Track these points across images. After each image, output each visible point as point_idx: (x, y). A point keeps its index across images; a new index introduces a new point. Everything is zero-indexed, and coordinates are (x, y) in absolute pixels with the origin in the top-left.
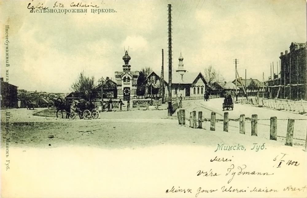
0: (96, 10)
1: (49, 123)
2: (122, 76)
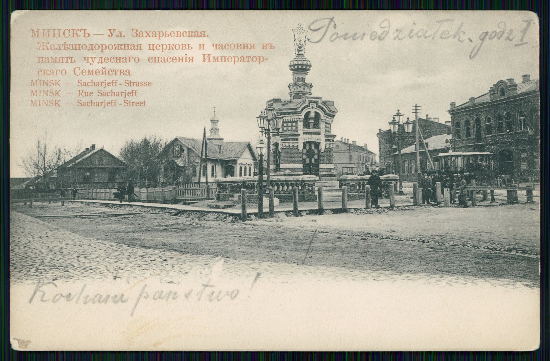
0: (158, 46)
1: (401, 253)
2: (302, 110)
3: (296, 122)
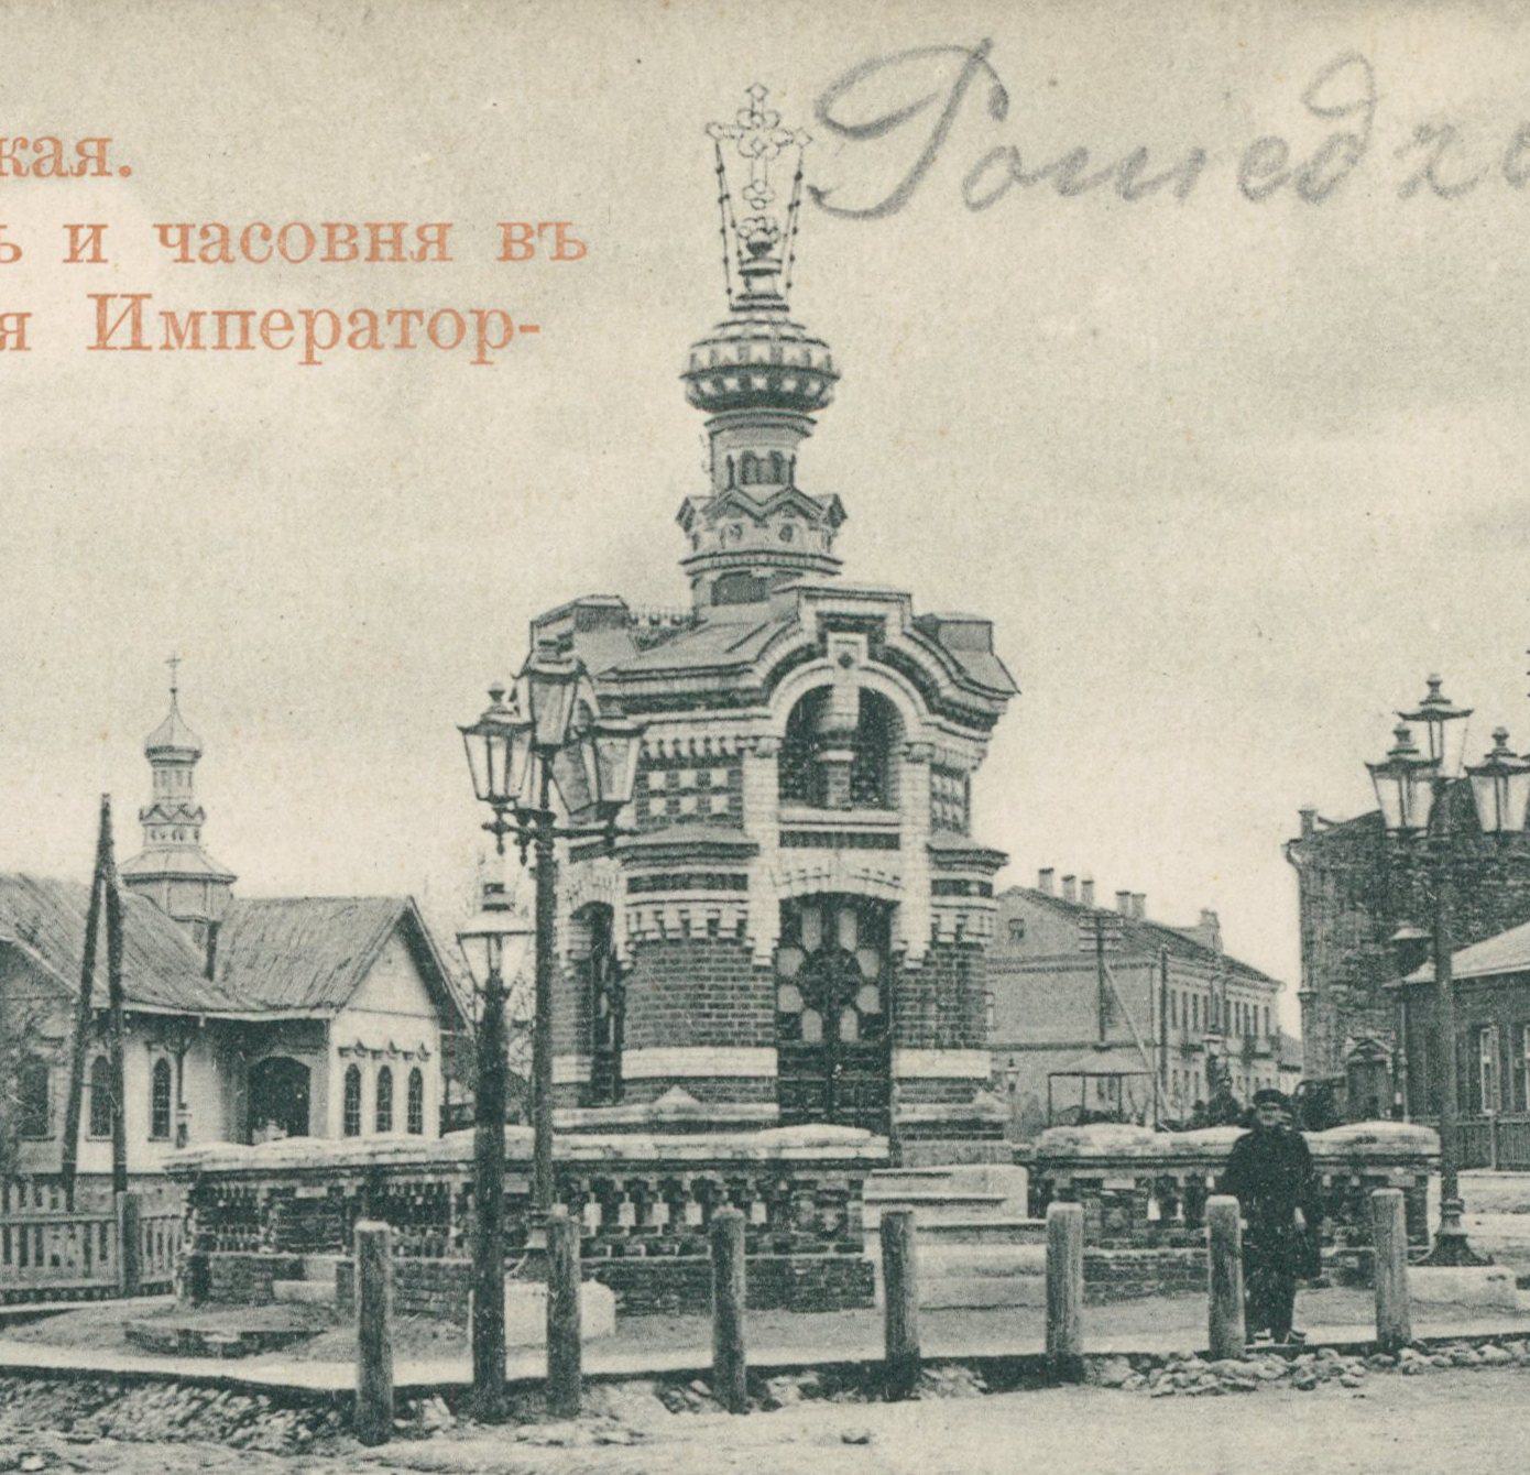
3: (733, 761)
